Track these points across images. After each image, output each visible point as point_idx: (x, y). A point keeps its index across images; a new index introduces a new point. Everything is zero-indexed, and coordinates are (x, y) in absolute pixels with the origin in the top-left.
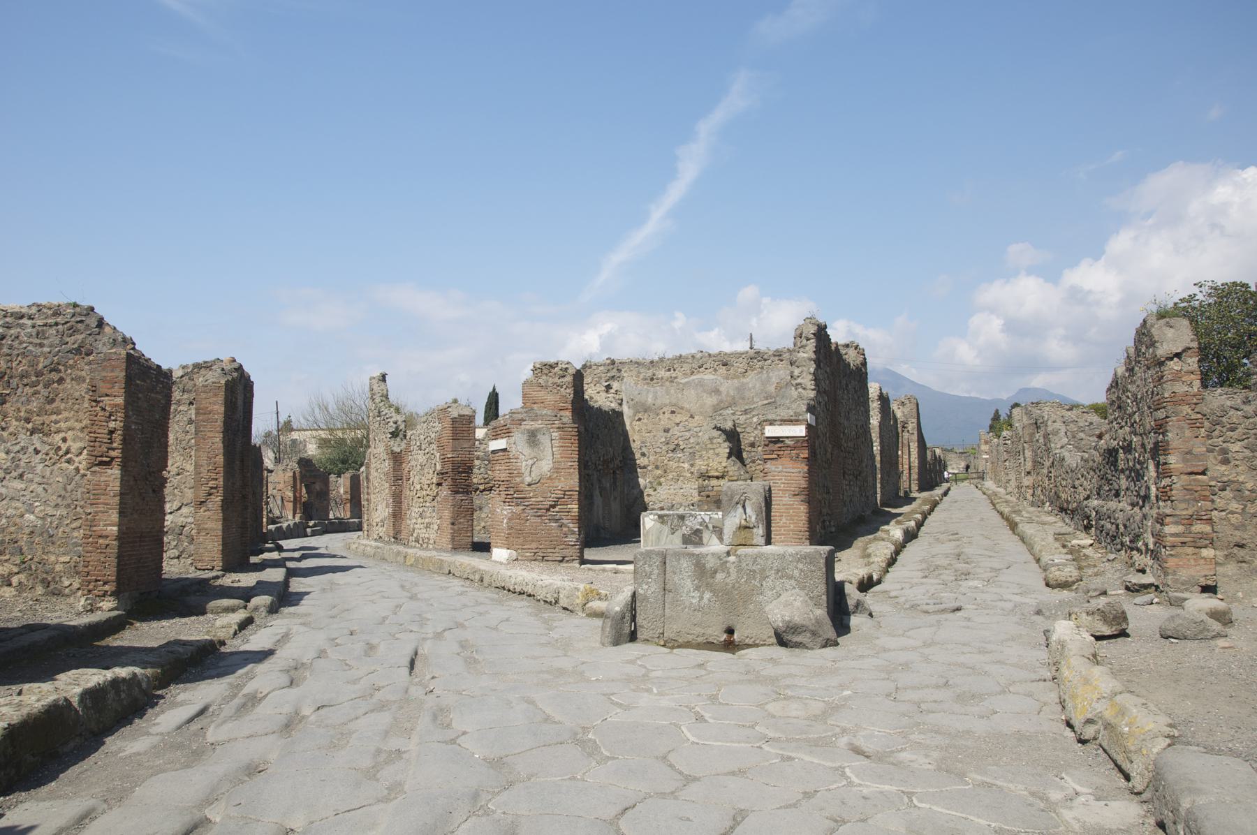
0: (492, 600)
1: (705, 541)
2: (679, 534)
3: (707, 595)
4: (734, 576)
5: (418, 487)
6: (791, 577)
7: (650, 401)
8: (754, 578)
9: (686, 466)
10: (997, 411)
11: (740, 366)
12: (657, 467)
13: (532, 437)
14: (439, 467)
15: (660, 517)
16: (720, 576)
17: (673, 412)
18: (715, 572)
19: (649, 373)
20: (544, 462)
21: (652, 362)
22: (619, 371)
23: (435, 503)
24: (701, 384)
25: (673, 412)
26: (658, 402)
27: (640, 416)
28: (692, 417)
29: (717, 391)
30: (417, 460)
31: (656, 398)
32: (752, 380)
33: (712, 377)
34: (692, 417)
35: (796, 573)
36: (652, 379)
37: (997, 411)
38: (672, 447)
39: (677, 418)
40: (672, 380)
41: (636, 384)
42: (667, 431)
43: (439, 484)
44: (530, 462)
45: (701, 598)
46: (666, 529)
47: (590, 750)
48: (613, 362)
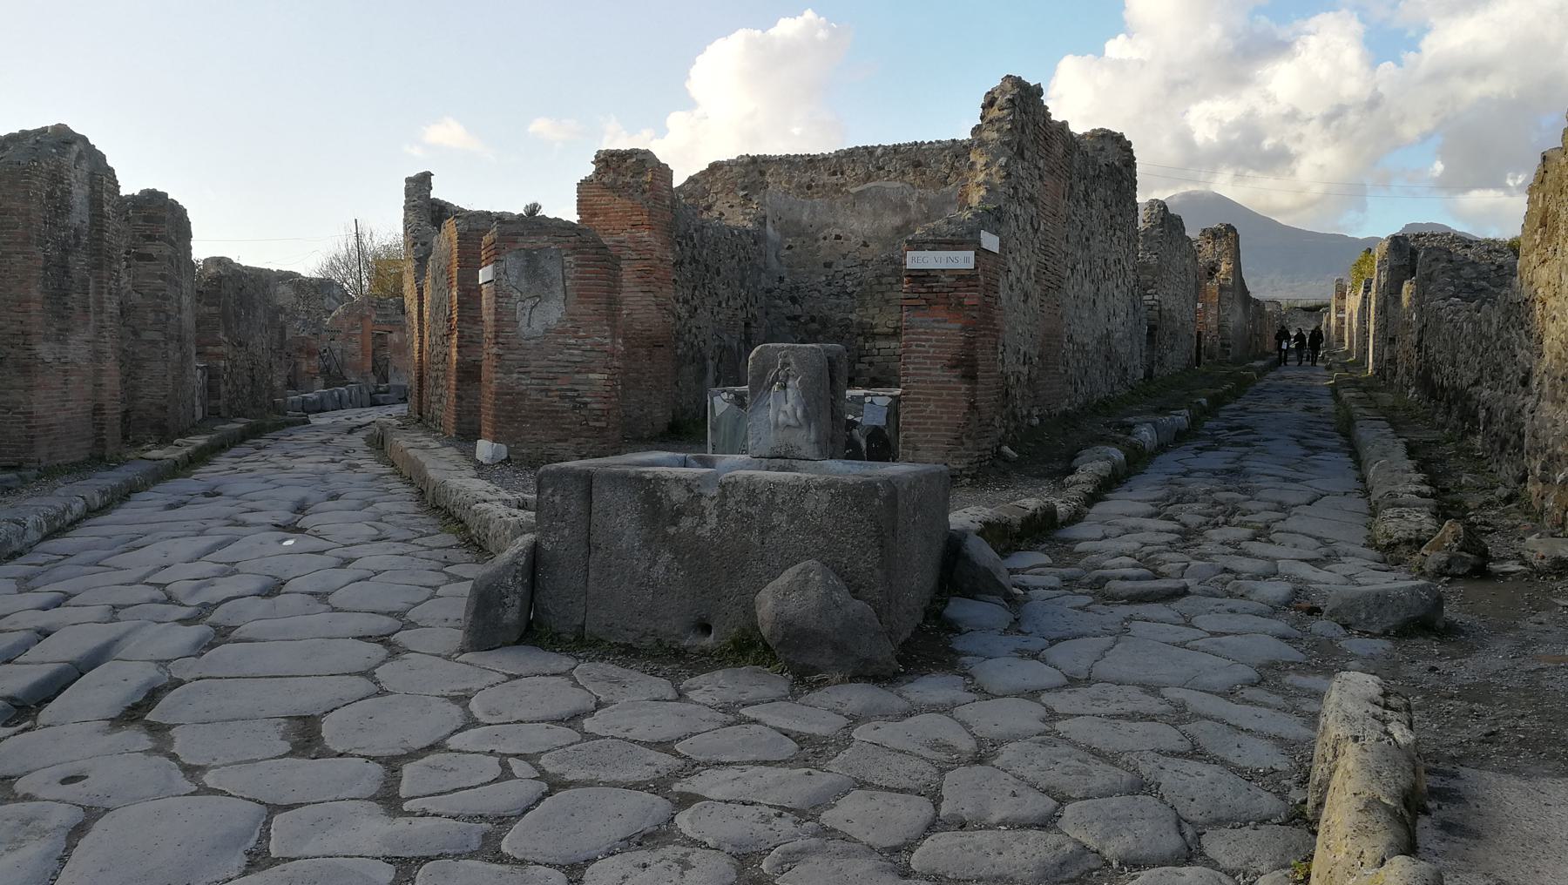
4: (713, 521)
12: (813, 319)
16: (686, 523)
17: (838, 237)
29: (904, 207)
31: (813, 212)
33: (898, 184)
36: (809, 187)
38: (835, 291)
40: (837, 188)
42: (828, 265)
44: (530, 303)
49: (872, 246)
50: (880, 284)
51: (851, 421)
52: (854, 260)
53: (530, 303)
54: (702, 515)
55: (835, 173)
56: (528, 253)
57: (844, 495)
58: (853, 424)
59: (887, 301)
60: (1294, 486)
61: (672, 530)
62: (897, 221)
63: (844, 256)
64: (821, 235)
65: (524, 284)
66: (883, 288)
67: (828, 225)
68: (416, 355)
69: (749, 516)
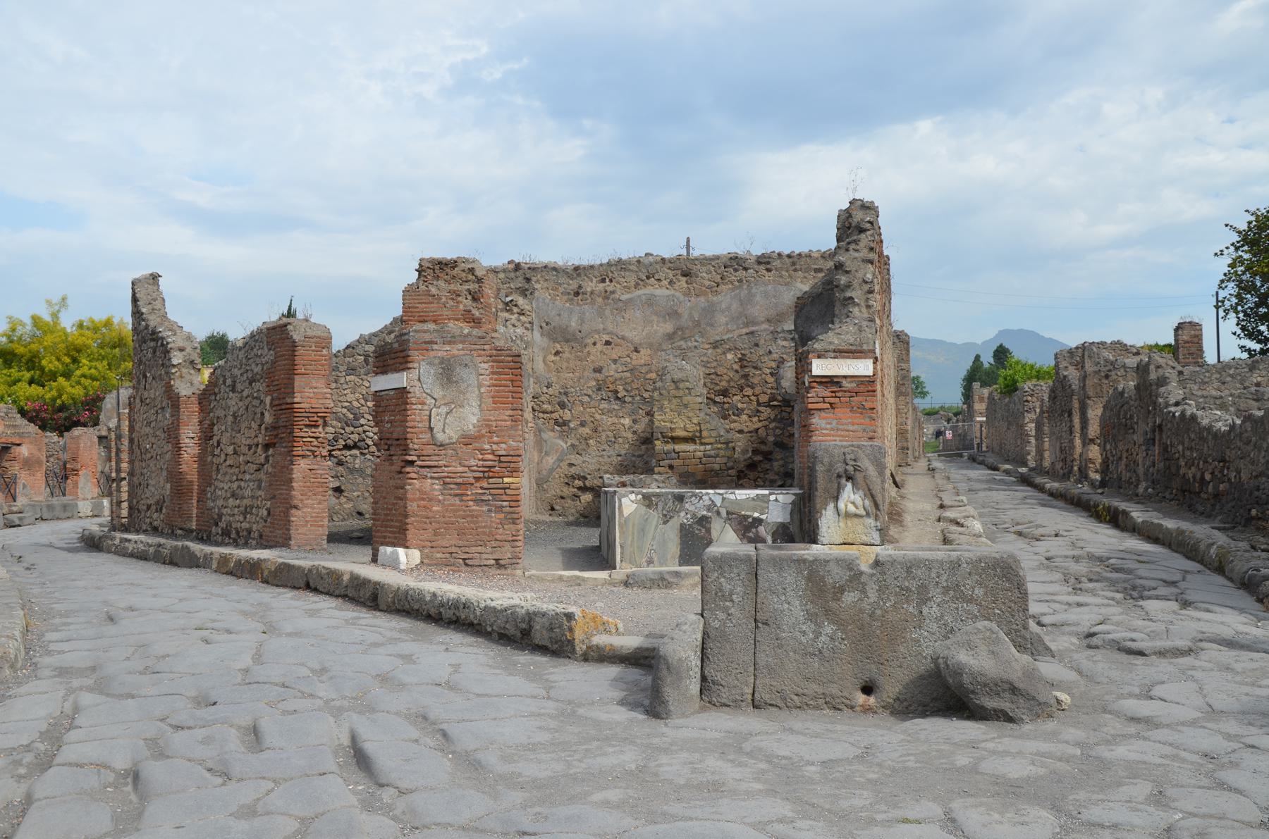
0: (401, 630)
1: (714, 534)
2: (675, 523)
3: (828, 629)
5: (230, 450)
6: (970, 600)
7: (574, 324)
8: (908, 601)
9: (627, 421)
10: (977, 358)
11: (705, 277)
12: (583, 424)
13: (447, 373)
14: (268, 418)
15: (646, 497)
16: (849, 597)
17: (608, 343)
18: (842, 590)
19: (574, 285)
20: (467, 410)
21: (577, 269)
22: (528, 280)
23: (262, 475)
24: (650, 302)
25: (608, 343)
26: (586, 328)
27: (558, 347)
28: (636, 350)
29: (673, 314)
30: (227, 408)
32: (726, 299)
33: (668, 292)
34: (636, 350)
35: (979, 592)
36: (577, 294)
37: (977, 358)
39: (614, 353)
40: (607, 295)
41: (553, 299)
42: (598, 370)
43: (267, 447)
44: (444, 410)
45: (818, 634)
46: (655, 516)
47: (227, 776)
48: (518, 267)
49: (643, 351)
50: (677, 388)
51: (754, 519)
52: (625, 365)
53: (444, 410)
54: (864, 591)
55: (603, 281)
56: (442, 361)
57: (994, 569)
58: (758, 522)
59: (686, 406)
60: (1147, 566)
61: (833, 605)
62: (668, 327)
63: (615, 361)
64: (590, 341)
65: (438, 392)
66: (681, 393)
67: (597, 332)
68: (1046, 445)
69: (908, 589)
